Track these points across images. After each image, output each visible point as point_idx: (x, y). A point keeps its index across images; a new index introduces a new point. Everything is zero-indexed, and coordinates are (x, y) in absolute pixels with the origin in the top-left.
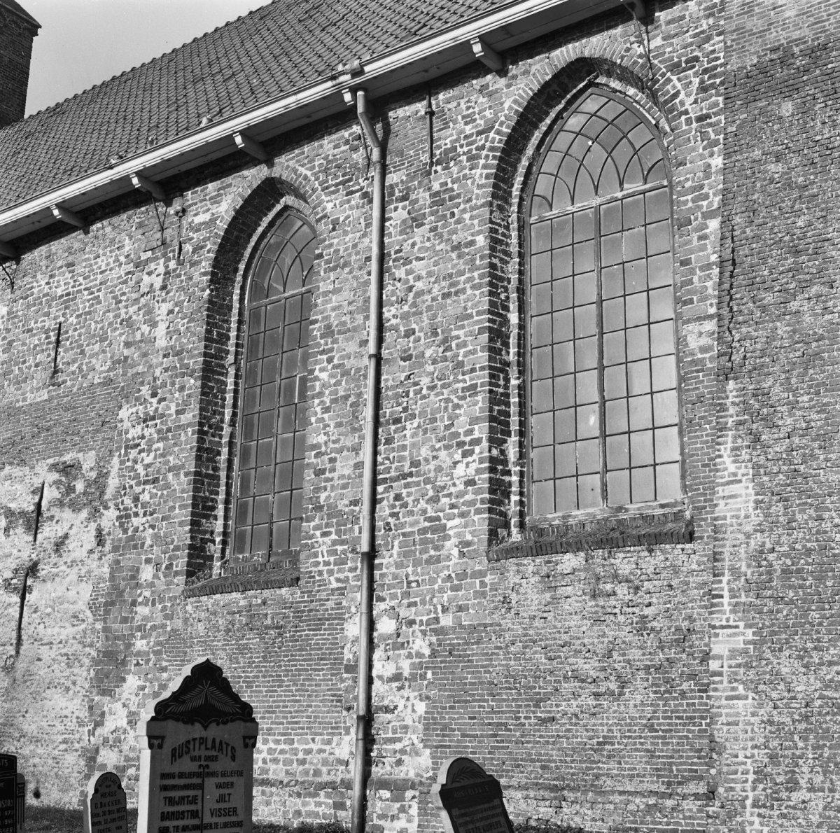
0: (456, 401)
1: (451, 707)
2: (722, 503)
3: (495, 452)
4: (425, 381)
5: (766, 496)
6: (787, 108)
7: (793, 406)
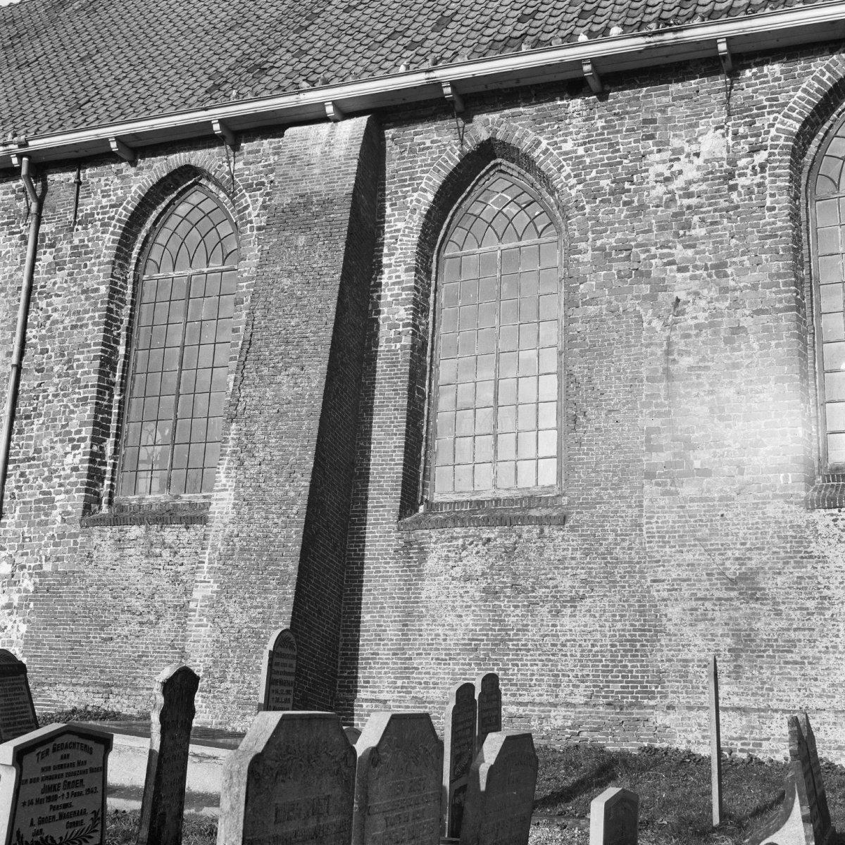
0: (72, 407)
1: (44, 629)
2: (214, 503)
3: (95, 448)
4: (51, 390)
5: (243, 501)
6: (301, 240)
7: (266, 445)
